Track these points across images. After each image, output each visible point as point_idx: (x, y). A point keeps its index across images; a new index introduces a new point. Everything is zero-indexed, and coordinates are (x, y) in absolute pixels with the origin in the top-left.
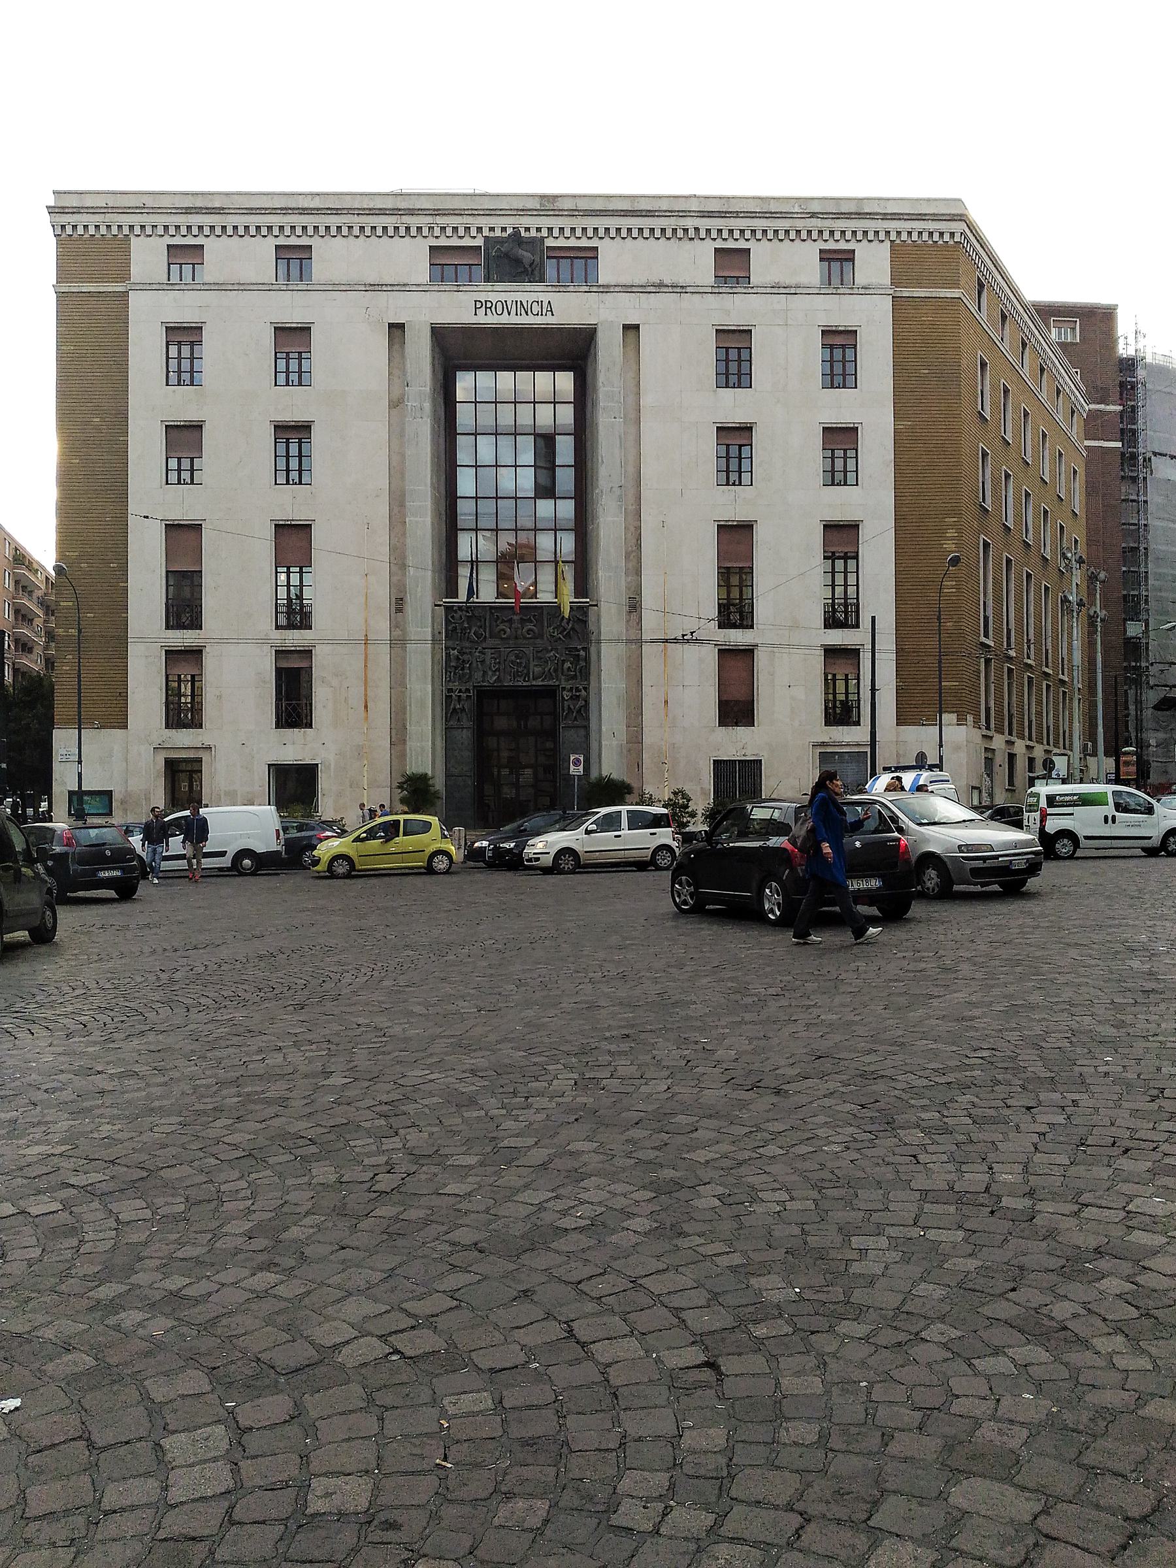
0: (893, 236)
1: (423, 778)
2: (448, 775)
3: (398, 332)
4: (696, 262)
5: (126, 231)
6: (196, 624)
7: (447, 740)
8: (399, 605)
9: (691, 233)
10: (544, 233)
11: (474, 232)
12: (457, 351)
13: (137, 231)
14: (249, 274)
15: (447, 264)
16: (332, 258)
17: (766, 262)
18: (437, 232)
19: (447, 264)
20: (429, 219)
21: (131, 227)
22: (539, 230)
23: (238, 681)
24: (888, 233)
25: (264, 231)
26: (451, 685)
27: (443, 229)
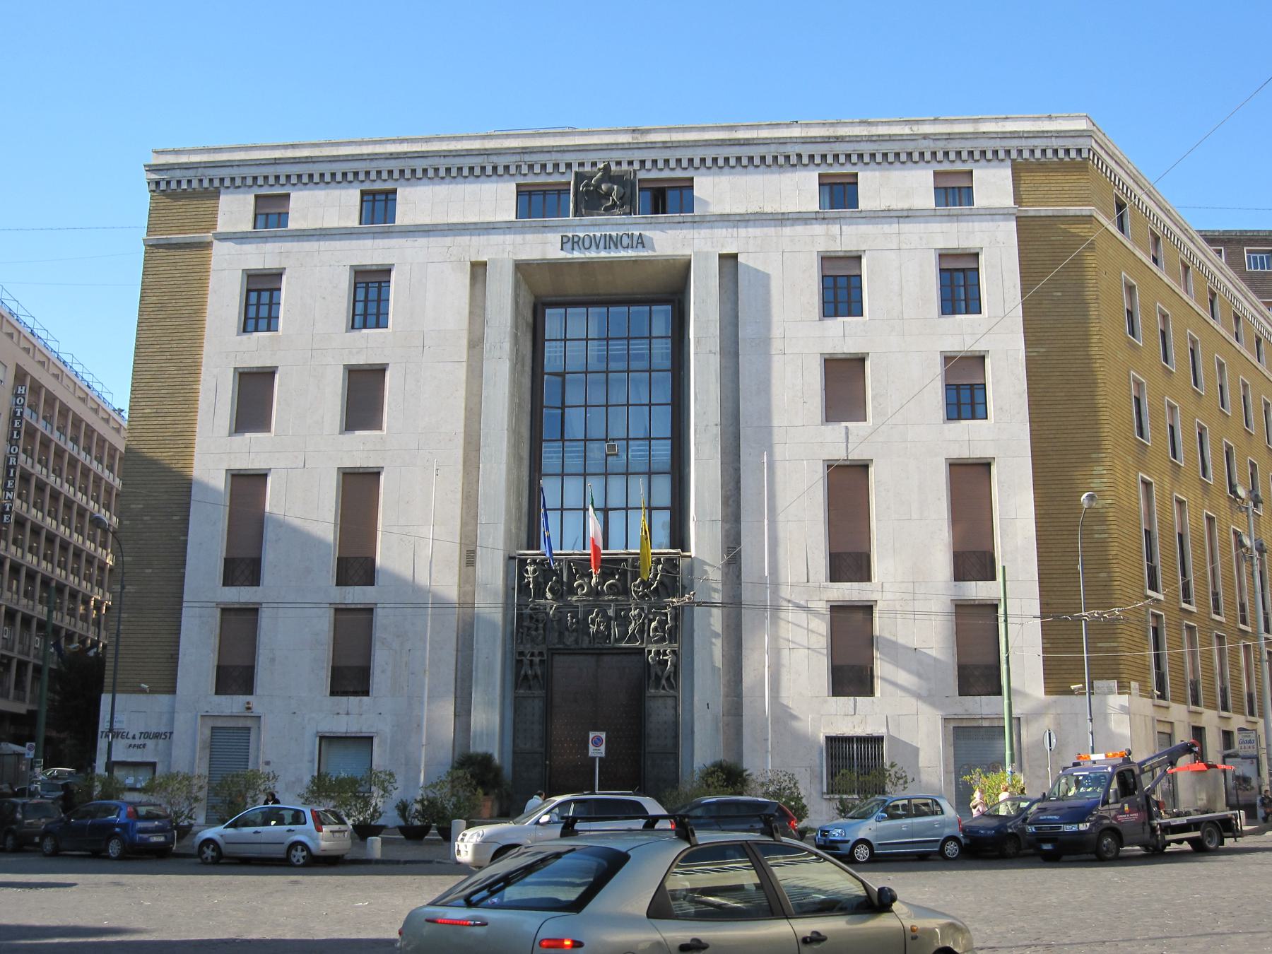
0: (1014, 155)
1: (486, 759)
2: (514, 765)
3: (480, 271)
4: (800, 191)
5: (216, 183)
6: (255, 580)
7: (516, 710)
8: (469, 558)
9: (794, 160)
10: (636, 166)
11: (563, 169)
12: (544, 293)
13: (227, 183)
14: (332, 221)
15: (536, 202)
16: (415, 203)
17: (874, 188)
18: (525, 170)
19: (536, 202)
20: (516, 158)
21: (222, 180)
22: (631, 163)
23: (294, 644)
24: (1008, 152)
25: (350, 177)
26: (521, 648)
27: (531, 167)
